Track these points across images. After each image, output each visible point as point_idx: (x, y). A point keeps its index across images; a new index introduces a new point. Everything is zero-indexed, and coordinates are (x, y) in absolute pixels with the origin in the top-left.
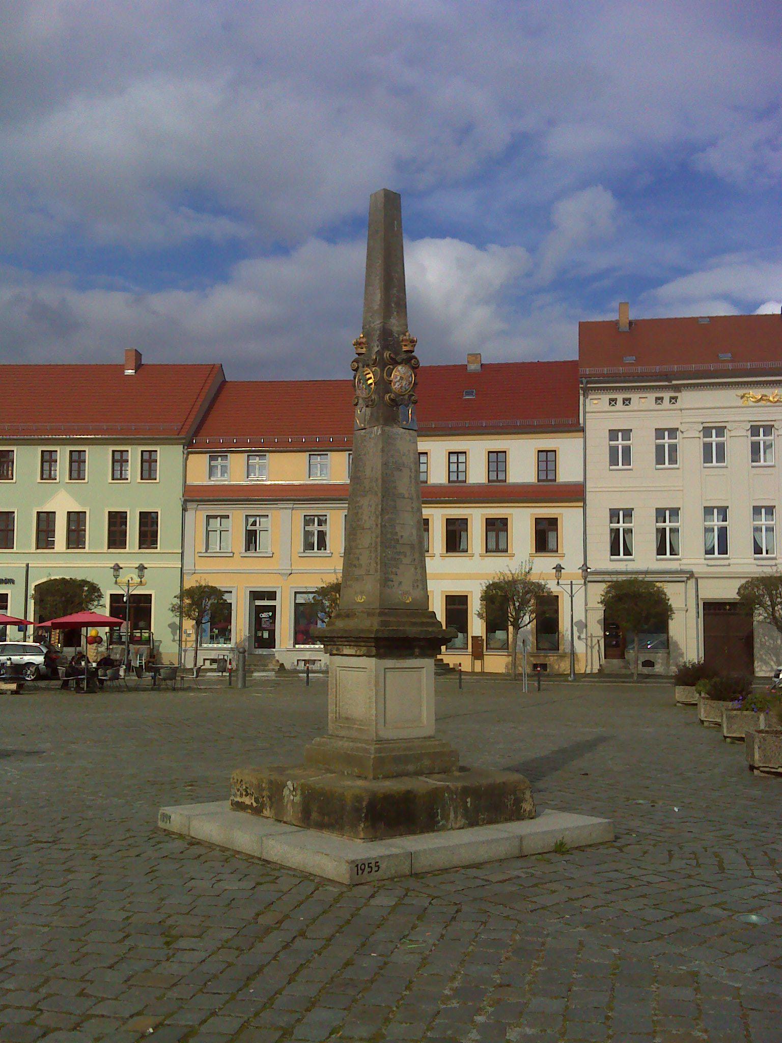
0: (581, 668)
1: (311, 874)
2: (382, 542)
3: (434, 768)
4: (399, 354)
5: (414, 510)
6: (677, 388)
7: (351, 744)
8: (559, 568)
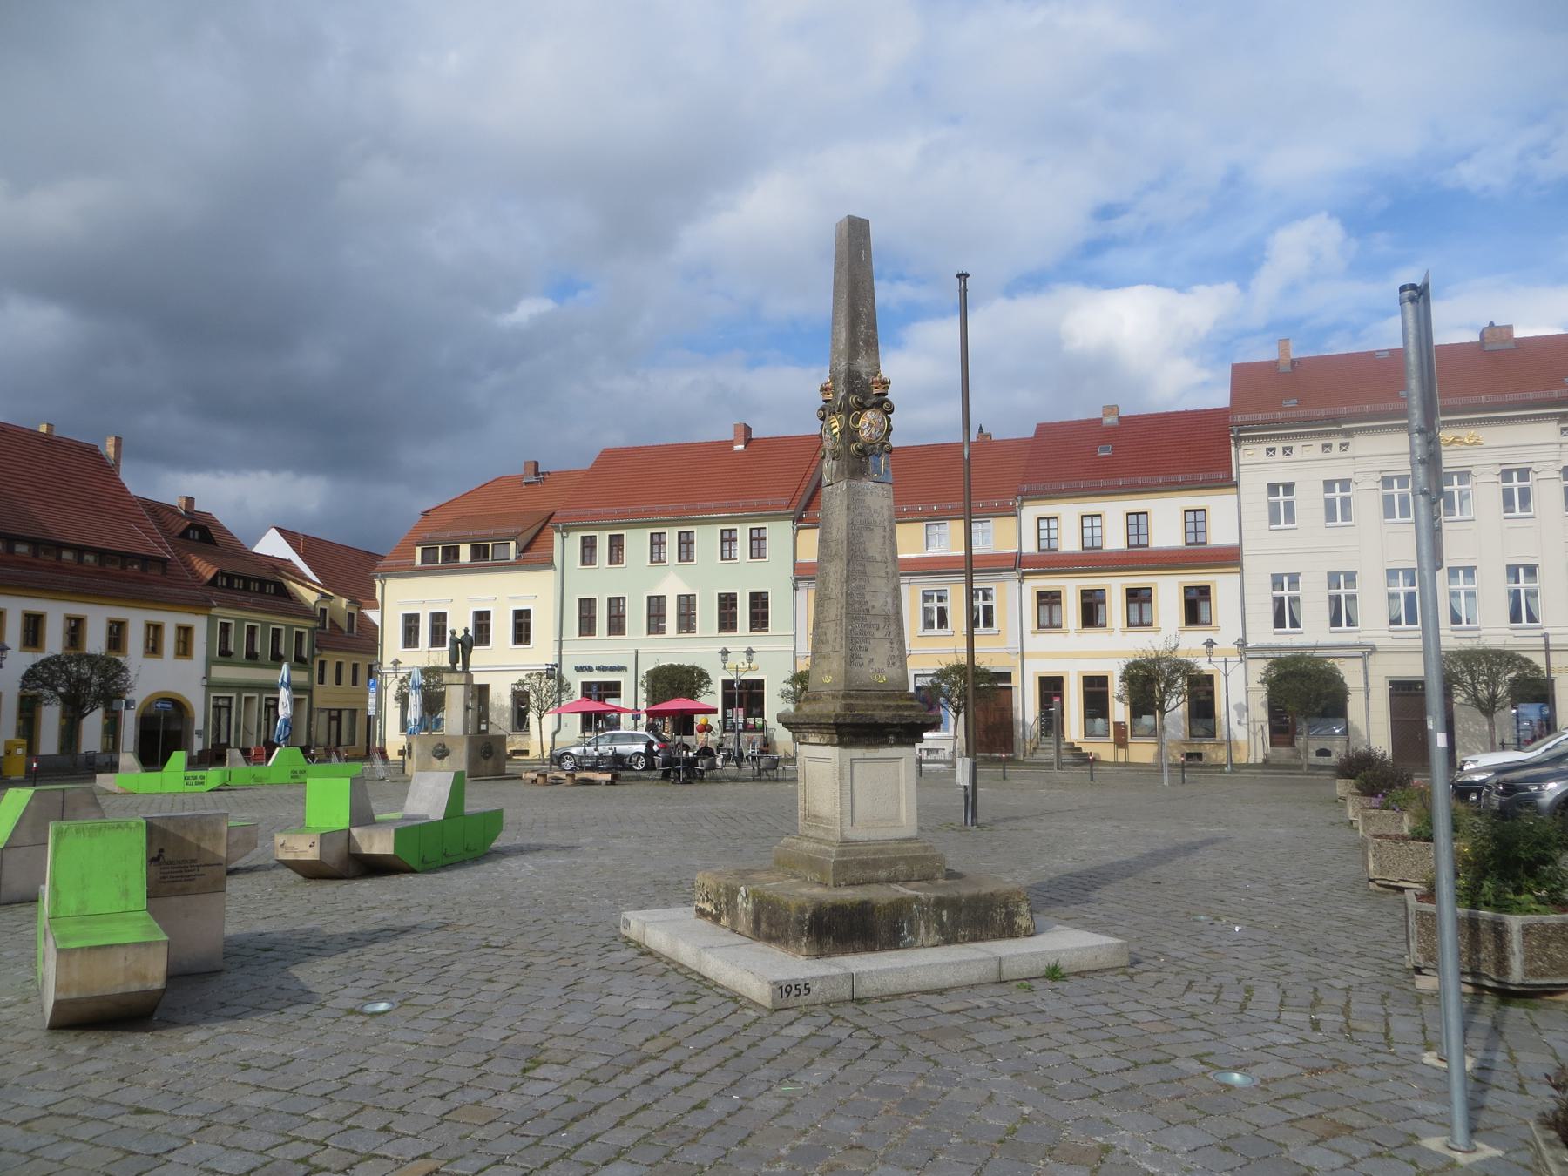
0: (1241, 757)
1: (740, 995)
2: (847, 614)
4: (868, 398)
6: (1348, 433)
7: (816, 845)
8: (1210, 644)
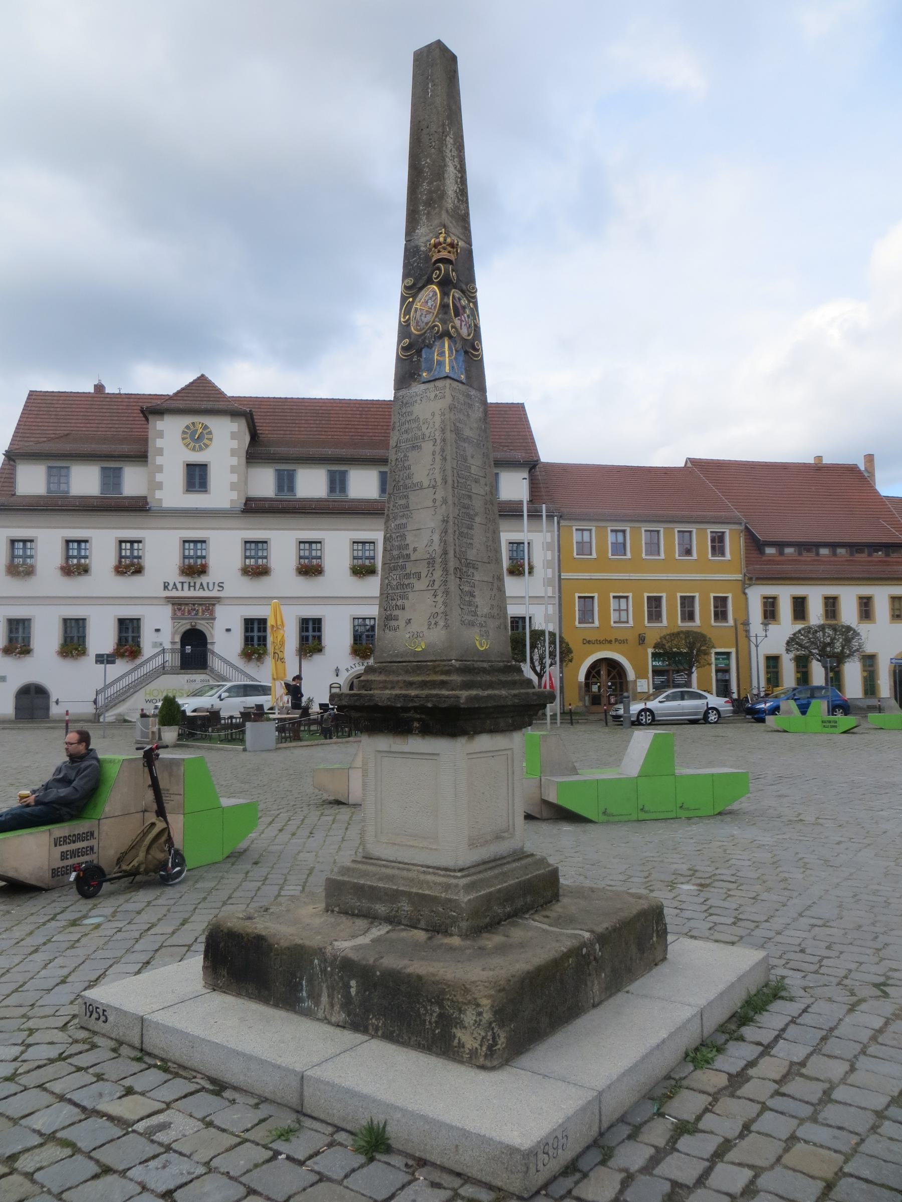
3: (419, 920)
5: (438, 503)
